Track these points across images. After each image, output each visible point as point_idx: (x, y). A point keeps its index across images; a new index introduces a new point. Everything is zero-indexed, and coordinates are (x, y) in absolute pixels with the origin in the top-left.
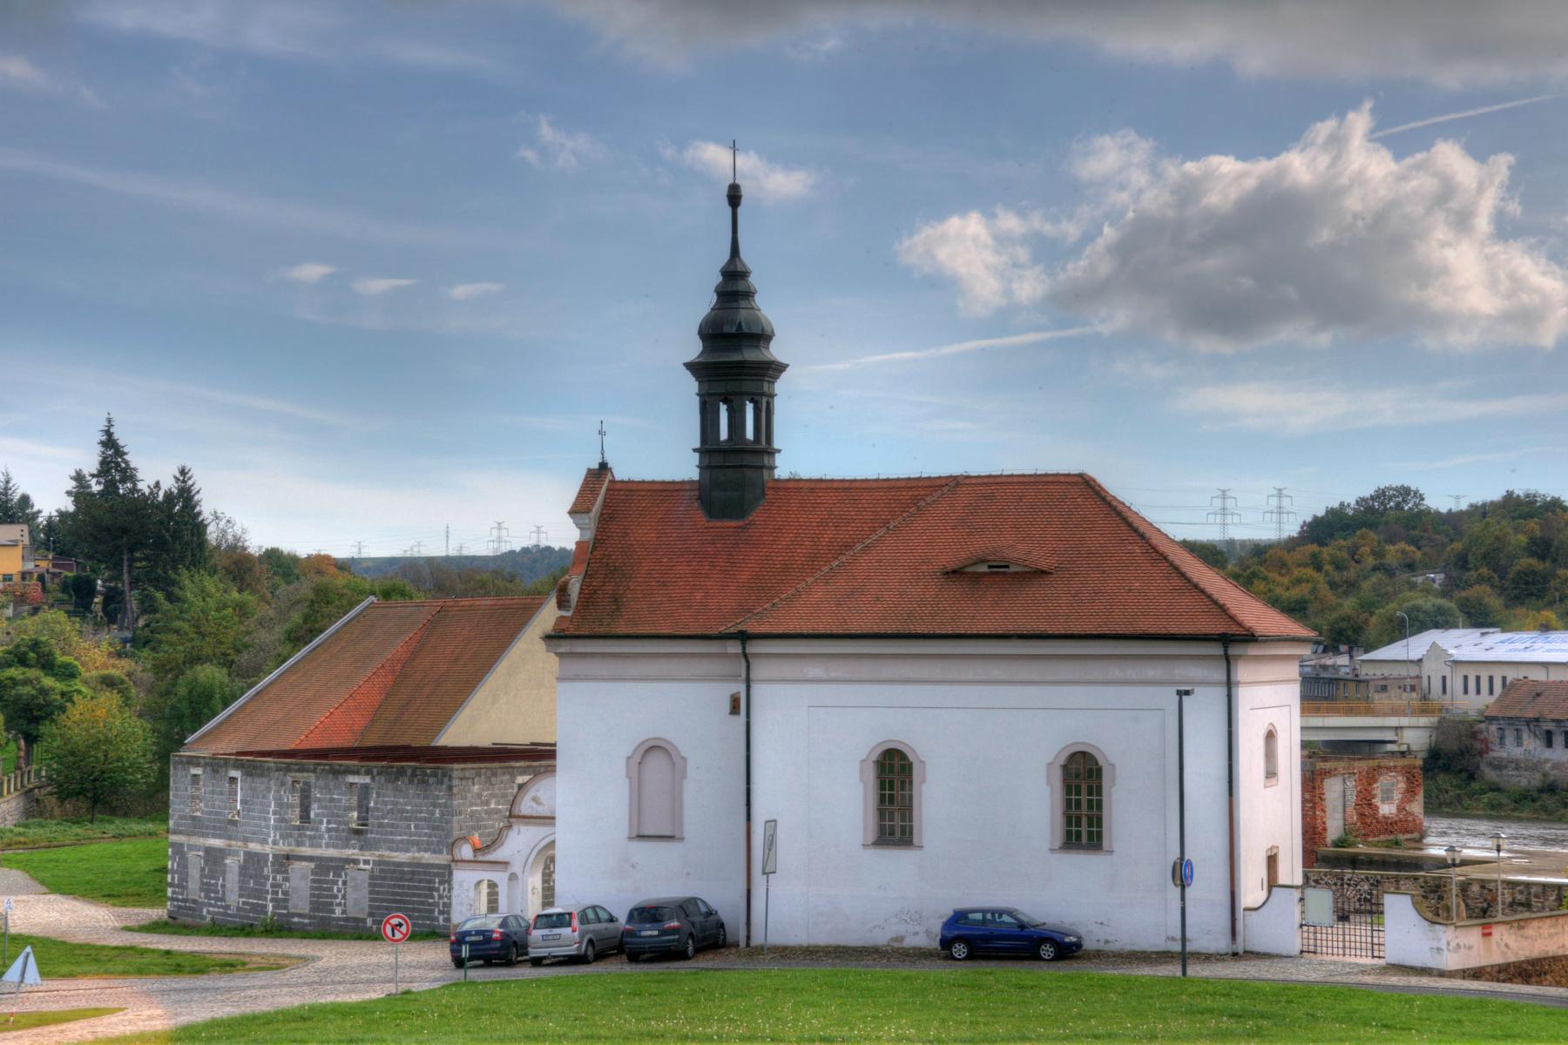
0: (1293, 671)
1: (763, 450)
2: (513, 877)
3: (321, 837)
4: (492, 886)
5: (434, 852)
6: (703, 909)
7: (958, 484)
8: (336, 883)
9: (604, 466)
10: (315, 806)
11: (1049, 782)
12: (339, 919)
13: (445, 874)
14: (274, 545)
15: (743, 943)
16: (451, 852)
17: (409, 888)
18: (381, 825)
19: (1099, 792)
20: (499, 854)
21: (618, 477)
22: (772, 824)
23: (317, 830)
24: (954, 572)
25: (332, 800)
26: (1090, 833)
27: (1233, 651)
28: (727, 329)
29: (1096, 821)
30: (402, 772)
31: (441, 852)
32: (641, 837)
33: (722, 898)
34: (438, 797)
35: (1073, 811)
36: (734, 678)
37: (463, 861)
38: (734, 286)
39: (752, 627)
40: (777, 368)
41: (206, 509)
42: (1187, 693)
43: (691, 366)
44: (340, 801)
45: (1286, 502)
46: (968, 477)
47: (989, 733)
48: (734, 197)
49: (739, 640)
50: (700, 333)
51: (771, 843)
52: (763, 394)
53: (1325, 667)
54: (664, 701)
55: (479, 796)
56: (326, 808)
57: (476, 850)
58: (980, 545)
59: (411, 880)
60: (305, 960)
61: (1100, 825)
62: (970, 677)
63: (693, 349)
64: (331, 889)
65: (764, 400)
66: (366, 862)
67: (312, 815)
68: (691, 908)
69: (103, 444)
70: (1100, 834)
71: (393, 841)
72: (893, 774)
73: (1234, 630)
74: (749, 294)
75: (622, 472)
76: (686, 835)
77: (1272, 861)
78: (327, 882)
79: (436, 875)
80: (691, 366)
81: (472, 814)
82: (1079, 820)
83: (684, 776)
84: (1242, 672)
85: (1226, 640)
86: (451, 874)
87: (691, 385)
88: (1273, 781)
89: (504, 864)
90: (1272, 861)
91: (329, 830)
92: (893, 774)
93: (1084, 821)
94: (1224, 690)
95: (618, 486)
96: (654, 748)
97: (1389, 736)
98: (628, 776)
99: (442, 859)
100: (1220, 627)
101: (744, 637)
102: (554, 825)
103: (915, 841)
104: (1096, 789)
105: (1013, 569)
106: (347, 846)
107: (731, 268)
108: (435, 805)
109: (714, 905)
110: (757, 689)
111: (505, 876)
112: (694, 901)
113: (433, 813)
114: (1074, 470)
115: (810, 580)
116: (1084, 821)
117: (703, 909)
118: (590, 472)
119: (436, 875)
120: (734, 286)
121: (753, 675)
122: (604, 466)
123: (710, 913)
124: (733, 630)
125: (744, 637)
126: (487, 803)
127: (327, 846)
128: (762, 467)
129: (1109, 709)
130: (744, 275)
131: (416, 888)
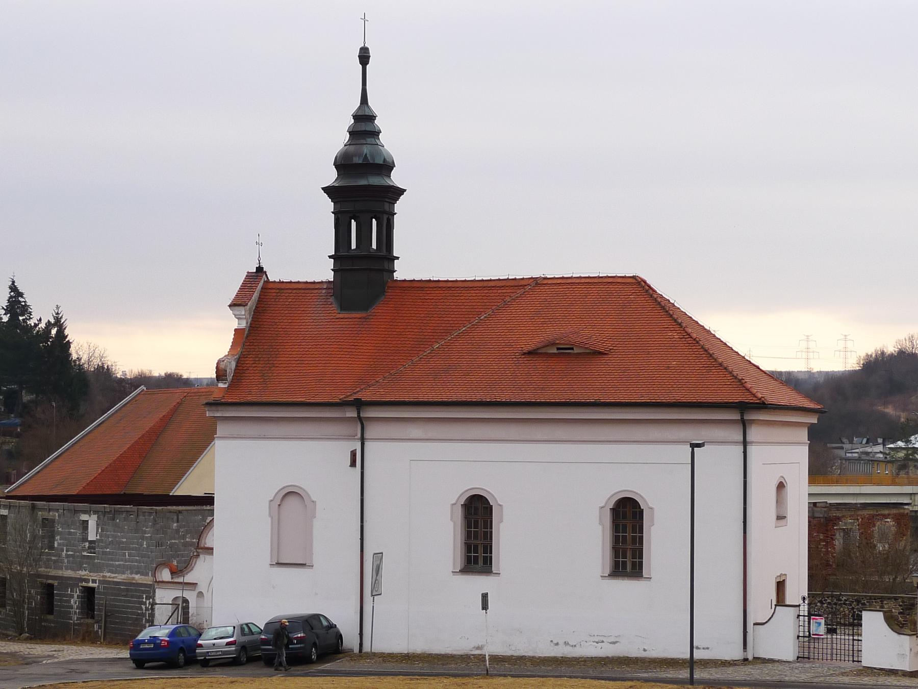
0: (803, 435)
1: (386, 257)
2: (200, 594)
3: (62, 562)
4: (186, 601)
5: (142, 574)
6: (325, 623)
7: (537, 284)
8: (72, 596)
9: (260, 270)
10: (58, 537)
11: (601, 523)
12: (75, 624)
13: (150, 590)
14: (170, 371)
15: (356, 650)
16: (154, 575)
17: (125, 601)
18: (104, 553)
19: (641, 531)
20: (189, 578)
21: (271, 279)
22: (379, 556)
23: (60, 556)
24: (530, 353)
25: (70, 533)
26: (634, 564)
27: (749, 416)
28: (357, 160)
29: (638, 553)
30: (117, 512)
31: (147, 575)
32: (279, 564)
33: (343, 617)
34: (145, 532)
35: (473, 541)
36: (351, 438)
37: (163, 582)
38: (364, 126)
39: (366, 396)
40: (400, 192)
41: (71, 333)
42: (699, 446)
43: (327, 190)
44: (75, 534)
45: (849, 344)
46: (546, 278)
47: (550, 483)
48: (364, 57)
49: (356, 409)
50: (335, 164)
51: (377, 570)
52: (385, 212)
53: (867, 454)
54: (308, 458)
55: (177, 531)
56: (65, 539)
57: (173, 573)
58: (550, 333)
59: (125, 596)
60: (27, 661)
61: (641, 557)
62: (539, 437)
63: (331, 176)
64: (69, 601)
65: (385, 217)
66: (94, 581)
67: (56, 545)
68: (314, 623)
69: (10, 288)
70: (641, 564)
71: (112, 565)
72: (477, 514)
73: (748, 399)
74: (376, 133)
75: (274, 275)
76: (315, 563)
77: (781, 586)
78: (66, 596)
79: (143, 592)
80: (327, 190)
81: (172, 546)
82: (476, 547)
83: (314, 516)
84: (754, 433)
85: (743, 407)
86: (154, 592)
87: (328, 205)
88: (782, 522)
89: (194, 585)
90: (781, 586)
91: (68, 556)
92: (477, 514)
93: (629, 554)
94: (741, 448)
95: (271, 286)
96: (291, 494)
97: (906, 500)
98: (270, 515)
99: (148, 580)
100: (737, 397)
101: (359, 404)
102: (212, 554)
103: (494, 569)
104: (638, 527)
105: (576, 351)
106: (81, 569)
107: (360, 114)
108: (143, 538)
109: (334, 621)
110: (368, 444)
111: (195, 593)
112: (317, 617)
113: (142, 545)
114: (629, 274)
115: (416, 359)
116: (629, 554)
117: (325, 623)
118: (249, 276)
119: (143, 592)
120: (364, 126)
121: (367, 436)
122: (260, 270)
123: (332, 626)
124: (351, 398)
125: (359, 404)
126: (184, 537)
127: (67, 569)
128: (382, 270)
129: (646, 464)
130: (371, 118)
131: (129, 602)
